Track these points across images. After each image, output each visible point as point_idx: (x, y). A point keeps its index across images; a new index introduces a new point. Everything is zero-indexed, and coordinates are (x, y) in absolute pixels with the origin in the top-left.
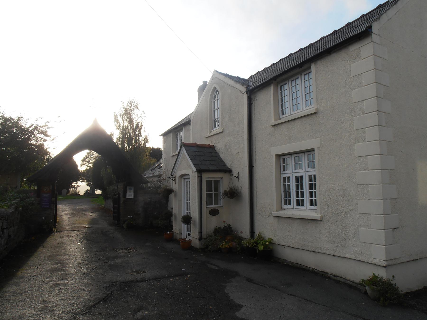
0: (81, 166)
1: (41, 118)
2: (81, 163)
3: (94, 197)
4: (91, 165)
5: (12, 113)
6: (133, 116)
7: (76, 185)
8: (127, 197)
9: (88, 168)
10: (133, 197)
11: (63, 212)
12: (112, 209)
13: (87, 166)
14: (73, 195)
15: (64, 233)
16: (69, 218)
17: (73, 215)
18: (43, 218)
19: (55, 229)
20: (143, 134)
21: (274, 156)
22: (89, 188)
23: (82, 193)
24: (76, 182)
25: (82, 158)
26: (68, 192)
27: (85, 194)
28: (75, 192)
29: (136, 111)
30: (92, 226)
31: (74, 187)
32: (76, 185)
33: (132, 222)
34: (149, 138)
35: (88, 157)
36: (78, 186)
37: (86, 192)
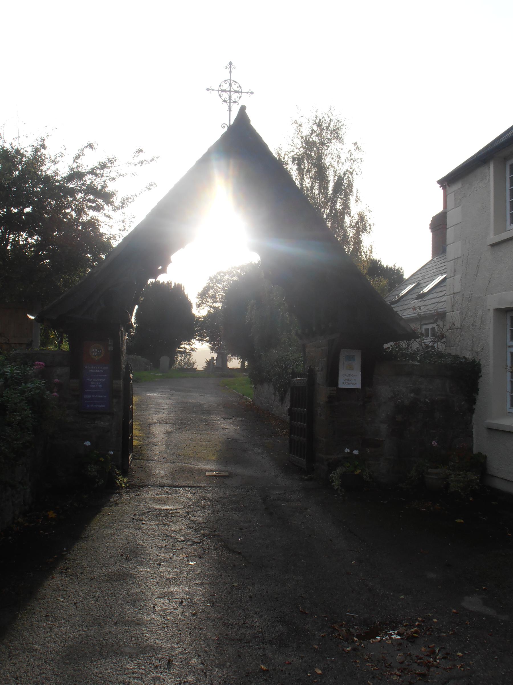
0: (199, 306)
1: (91, 146)
2: (197, 301)
3: (224, 376)
4: (218, 305)
5: (18, 137)
6: (327, 161)
7: (187, 347)
8: (341, 385)
9: (212, 311)
10: (358, 386)
11: (156, 412)
12: (288, 419)
13: (211, 307)
14: (182, 369)
15: (153, 493)
16: (168, 433)
17: (180, 424)
18: (88, 443)
19: (122, 480)
20: (355, 209)
21: (491, 314)
22: (215, 355)
23: (200, 365)
24: (189, 340)
25: (200, 290)
26: (172, 361)
27: (207, 368)
28: (187, 363)
29: (334, 147)
30: (231, 469)
31: (184, 352)
32: (187, 347)
33: (358, 472)
34: (370, 219)
35: (213, 288)
36: (192, 350)
37: (210, 363)
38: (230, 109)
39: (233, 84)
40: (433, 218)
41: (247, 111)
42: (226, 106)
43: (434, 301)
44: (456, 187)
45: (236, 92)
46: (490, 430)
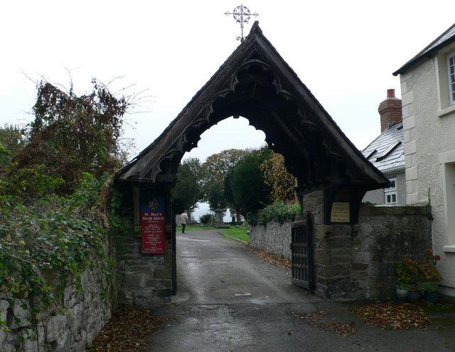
21: (443, 167)
38: (242, 27)
39: (244, 9)
40: (257, 129)
41: (259, 25)
42: (239, 24)
43: (393, 161)
44: (409, 76)
45: (246, 14)
46: (447, 253)
